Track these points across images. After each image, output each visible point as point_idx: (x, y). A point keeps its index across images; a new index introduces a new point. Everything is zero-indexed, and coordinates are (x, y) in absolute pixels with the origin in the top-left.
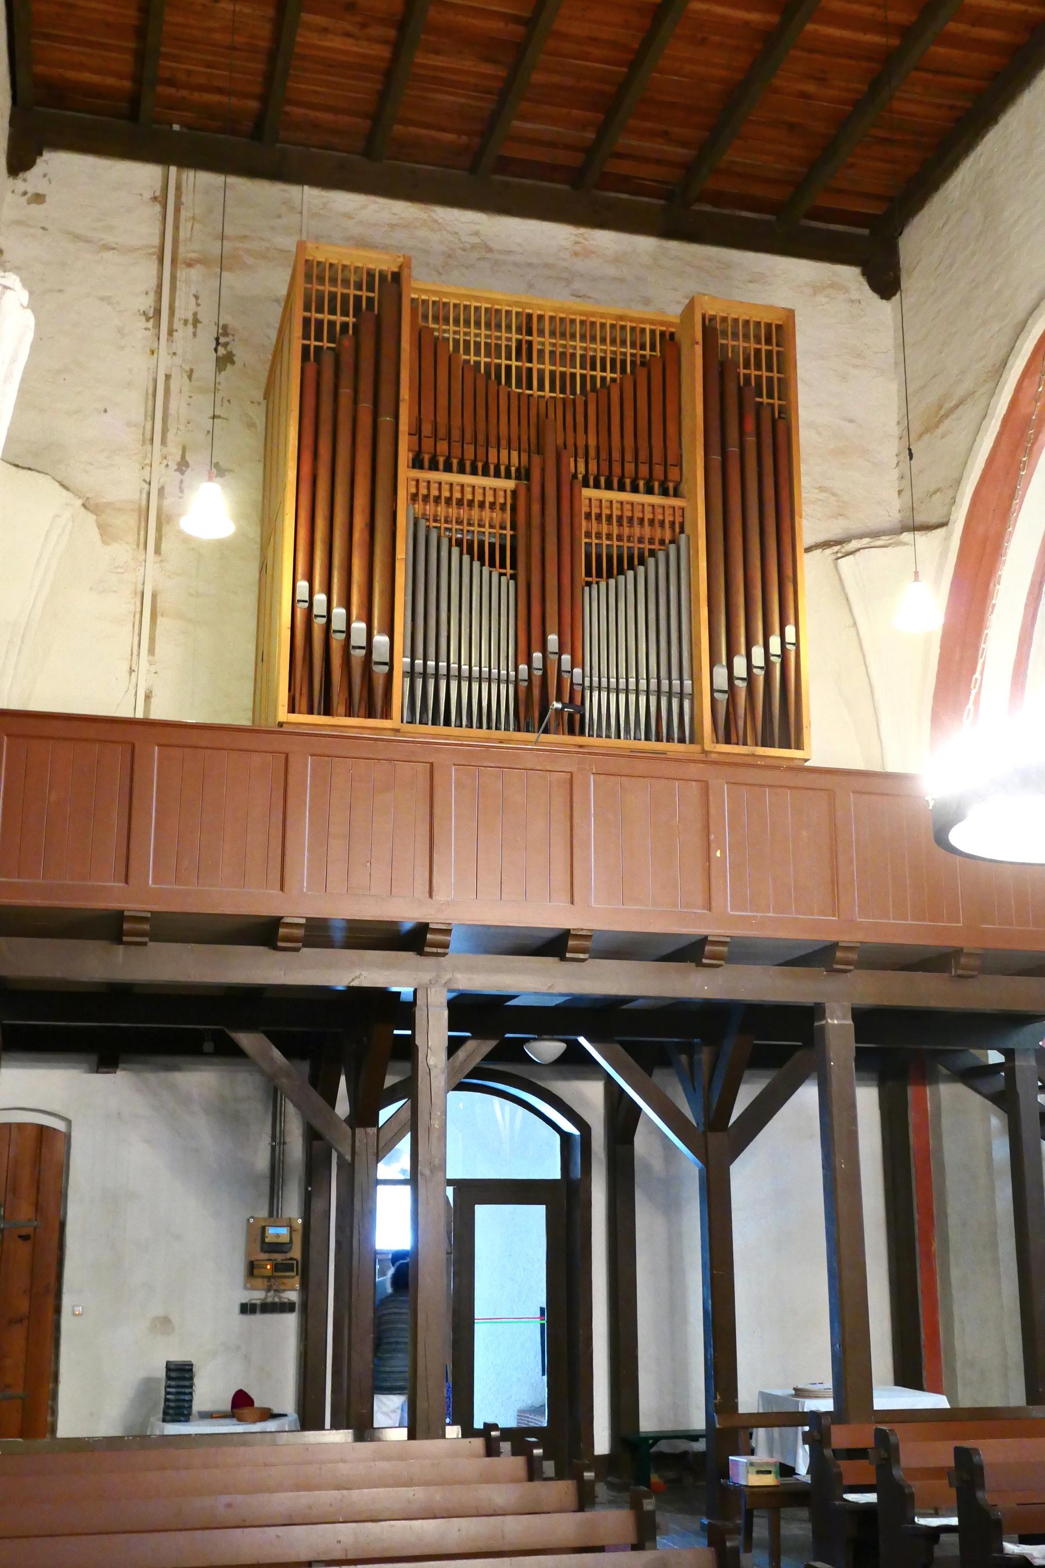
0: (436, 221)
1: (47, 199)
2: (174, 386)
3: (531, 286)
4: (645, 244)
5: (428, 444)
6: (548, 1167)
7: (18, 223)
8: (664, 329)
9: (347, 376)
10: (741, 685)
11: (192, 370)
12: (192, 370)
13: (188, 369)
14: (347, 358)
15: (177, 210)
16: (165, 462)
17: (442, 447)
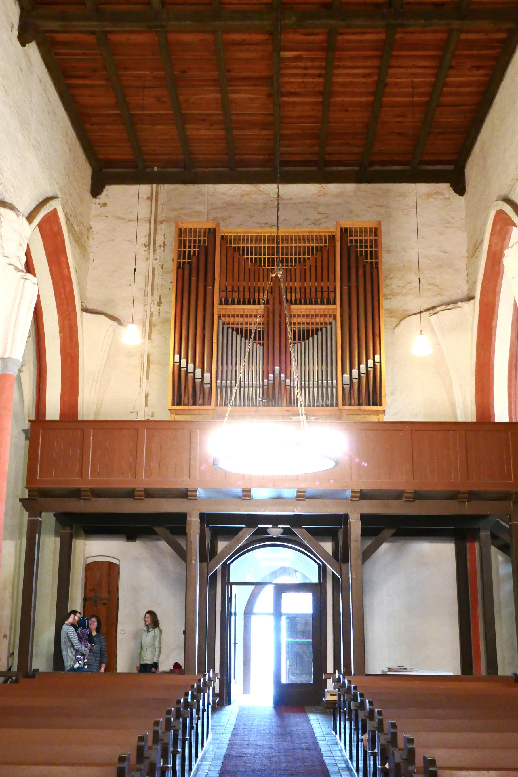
0: (260, 190)
1: (108, 205)
2: (156, 272)
3: (300, 212)
4: (350, 187)
5: (230, 294)
6: (314, 579)
7: (99, 215)
8: (330, 234)
9: (194, 273)
10: (364, 376)
11: (163, 265)
12: (163, 265)
13: (161, 264)
14: (194, 265)
15: (157, 201)
16: (153, 303)
17: (236, 295)
